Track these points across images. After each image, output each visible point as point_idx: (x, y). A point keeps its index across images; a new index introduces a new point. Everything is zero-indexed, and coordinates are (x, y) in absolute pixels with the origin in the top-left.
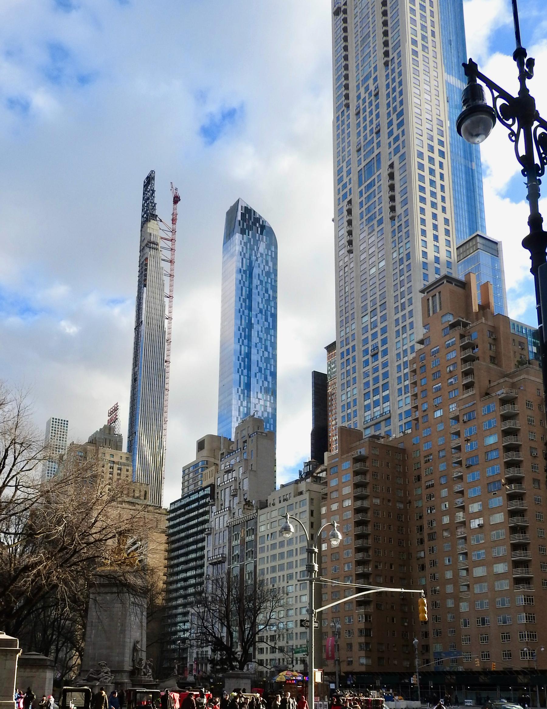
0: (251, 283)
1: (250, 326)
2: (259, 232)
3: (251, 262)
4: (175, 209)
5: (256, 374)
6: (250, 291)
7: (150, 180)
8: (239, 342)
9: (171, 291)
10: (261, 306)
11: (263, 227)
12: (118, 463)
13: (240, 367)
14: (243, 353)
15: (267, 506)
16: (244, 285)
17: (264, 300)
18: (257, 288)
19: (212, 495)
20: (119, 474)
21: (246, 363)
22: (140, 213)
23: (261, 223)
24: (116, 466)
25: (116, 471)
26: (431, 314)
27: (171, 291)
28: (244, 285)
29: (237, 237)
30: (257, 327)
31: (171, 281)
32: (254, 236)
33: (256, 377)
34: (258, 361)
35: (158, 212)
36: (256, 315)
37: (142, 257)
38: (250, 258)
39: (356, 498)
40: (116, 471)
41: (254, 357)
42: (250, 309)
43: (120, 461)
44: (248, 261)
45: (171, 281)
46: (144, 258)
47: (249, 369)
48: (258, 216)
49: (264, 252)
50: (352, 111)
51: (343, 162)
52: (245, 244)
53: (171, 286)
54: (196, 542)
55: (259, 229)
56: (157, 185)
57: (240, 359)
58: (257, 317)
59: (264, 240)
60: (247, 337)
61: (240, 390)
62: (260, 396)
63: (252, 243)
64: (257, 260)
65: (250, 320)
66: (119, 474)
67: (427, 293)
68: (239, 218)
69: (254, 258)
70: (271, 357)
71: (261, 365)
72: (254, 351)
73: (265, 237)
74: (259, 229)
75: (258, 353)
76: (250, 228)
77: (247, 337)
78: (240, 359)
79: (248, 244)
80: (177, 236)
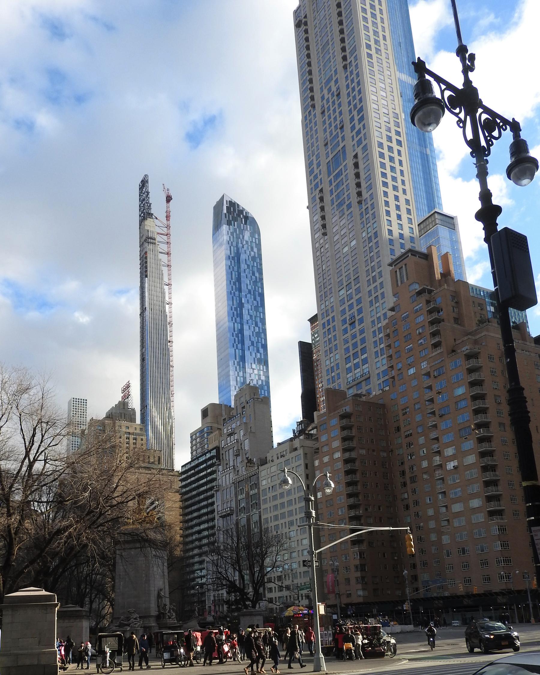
0: (239, 267)
2: (243, 223)
3: (238, 249)
4: (168, 207)
5: (249, 347)
6: (239, 274)
7: (144, 183)
8: (232, 320)
10: (249, 287)
11: (247, 218)
12: (133, 434)
14: (236, 329)
15: (267, 463)
16: (233, 270)
17: (251, 282)
19: (218, 456)
21: (240, 339)
22: (137, 213)
23: (244, 214)
24: (132, 437)
25: (132, 441)
26: (399, 284)
28: (233, 270)
29: (225, 228)
30: (247, 306)
32: (239, 227)
33: (249, 350)
35: (154, 210)
37: (142, 251)
38: (237, 245)
39: (345, 450)
40: (132, 441)
41: (247, 333)
42: (240, 290)
43: (135, 431)
44: (235, 248)
45: (169, 270)
46: (144, 252)
47: (243, 343)
49: (249, 239)
50: (318, 110)
51: (313, 156)
52: (232, 234)
53: (169, 275)
54: (206, 499)
55: (243, 220)
56: (151, 187)
57: (235, 335)
58: (246, 297)
60: (239, 315)
61: (236, 362)
63: (238, 233)
64: (243, 247)
65: (241, 300)
67: (395, 266)
69: (240, 245)
71: (253, 339)
72: (246, 327)
73: (248, 226)
74: (243, 220)
75: (249, 329)
76: (235, 219)
77: (239, 315)
78: (235, 335)
79: (235, 234)
80: (172, 231)
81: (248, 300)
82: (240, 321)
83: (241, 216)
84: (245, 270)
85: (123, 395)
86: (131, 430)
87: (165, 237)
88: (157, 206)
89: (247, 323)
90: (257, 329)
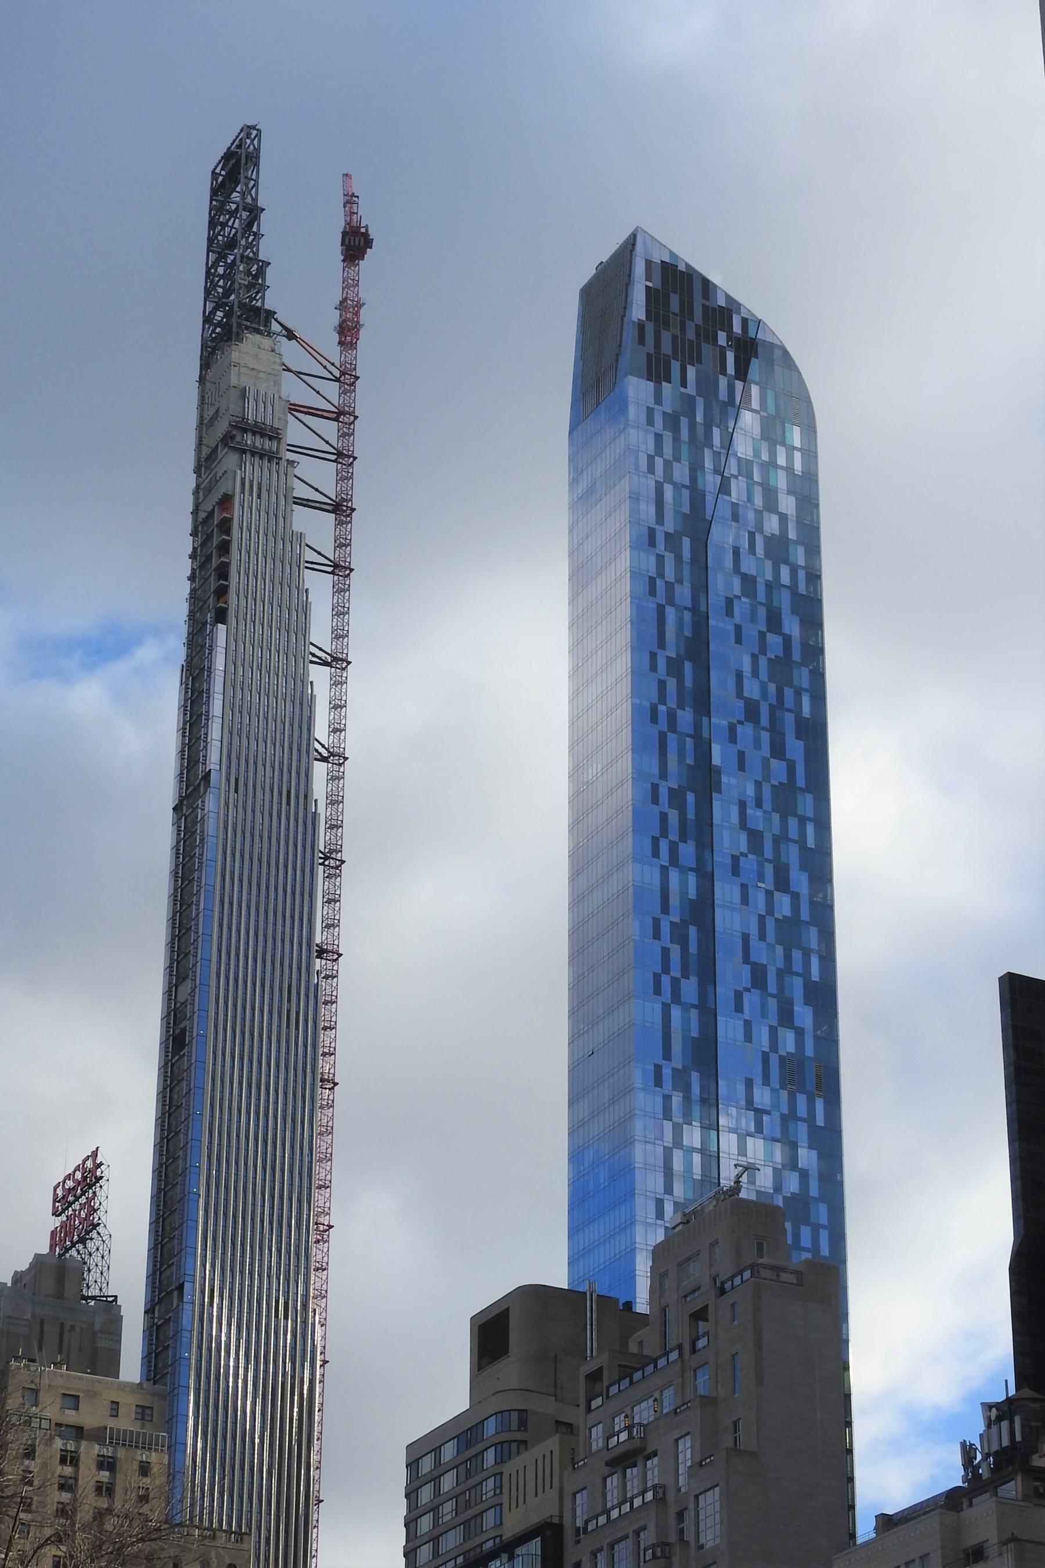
1: (705, 779)
2: (731, 369)
4: (350, 284)
9: (339, 635)
10: (752, 689)
12: (98, 1435)
13: (666, 968)
14: (674, 900)
17: (763, 662)
18: (729, 612)
20: (105, 1490)
23: (737, 328)
24: (90, 1452)
25: (89, 1475)
27: (339, 635)
29: (638, 390)
30: (735, 786)
31: (341, 590)
33: (739, 1008)
34: (746, 938)
36: (732, 729)
40: (89, 1475)
41: (730, 920)
42: (701, 702)
47: (708, 976)
48: (721, 302)
49: (757, 454)
53: (338, 706)
55: (730, 357)
57: (665, 929)
59: (755, 404)
61: (667, 1072)
62: (762, 1096)
64: (724, 488)
65: (703, 751)
66: (105, 1490)
68: (638, 311)
70: (805, 915)
71: (760, 953)
72: (726, 891)
73: (755, 390)
74: (730, 357)
76: (690, 354)
78: (665, 929)
79: (684, 422)
80: (363, 401)
81: (741, 755)
82: (699, 859)
83: (722, 338)
84: (735, 859)
85: (57, 1222)
86: (88, 1416)
87: (329, 429)
88: (299, 280)
89: (736, 871)
90: (788, 1042)
